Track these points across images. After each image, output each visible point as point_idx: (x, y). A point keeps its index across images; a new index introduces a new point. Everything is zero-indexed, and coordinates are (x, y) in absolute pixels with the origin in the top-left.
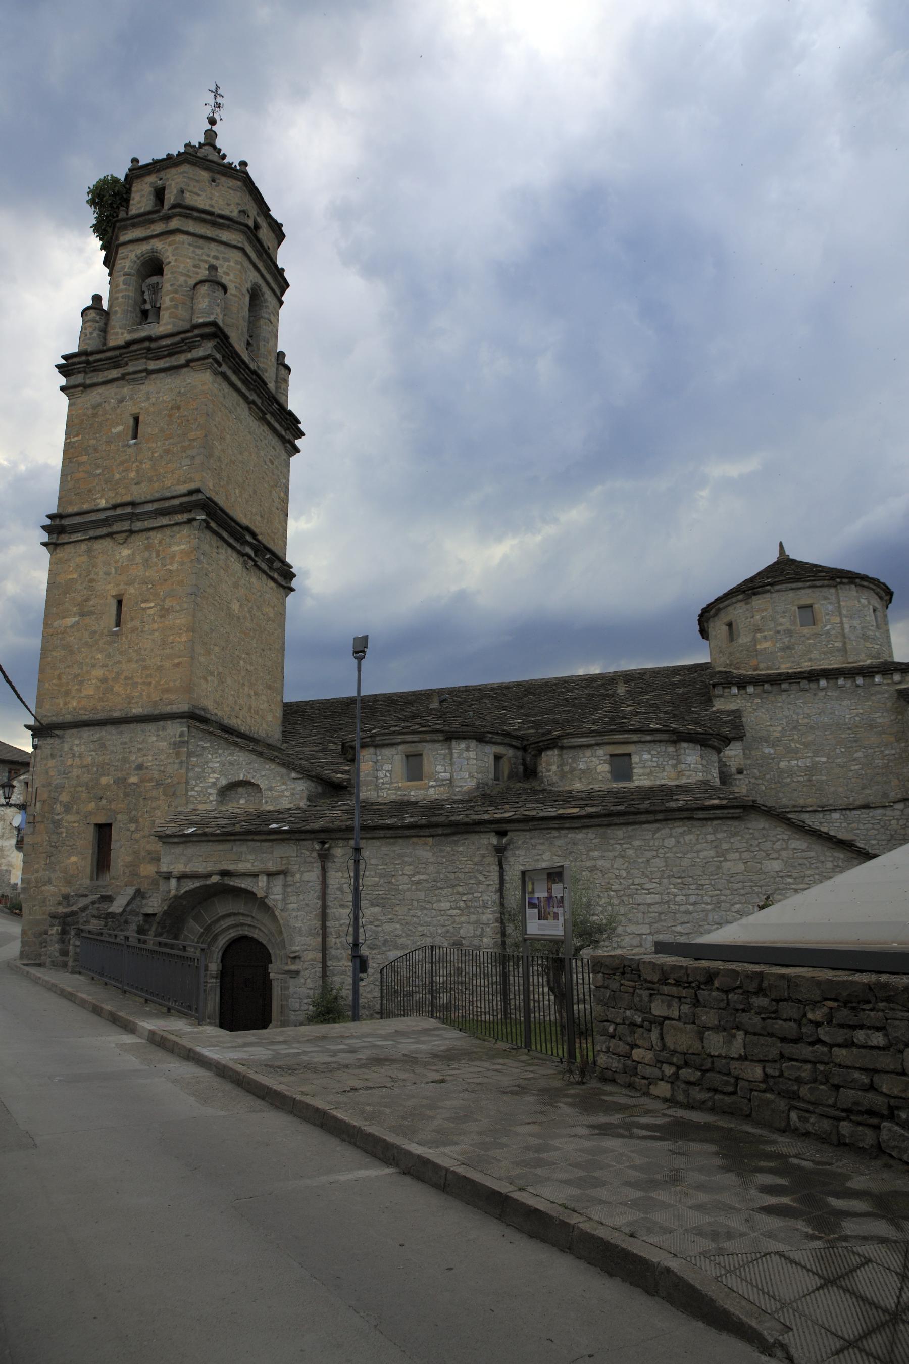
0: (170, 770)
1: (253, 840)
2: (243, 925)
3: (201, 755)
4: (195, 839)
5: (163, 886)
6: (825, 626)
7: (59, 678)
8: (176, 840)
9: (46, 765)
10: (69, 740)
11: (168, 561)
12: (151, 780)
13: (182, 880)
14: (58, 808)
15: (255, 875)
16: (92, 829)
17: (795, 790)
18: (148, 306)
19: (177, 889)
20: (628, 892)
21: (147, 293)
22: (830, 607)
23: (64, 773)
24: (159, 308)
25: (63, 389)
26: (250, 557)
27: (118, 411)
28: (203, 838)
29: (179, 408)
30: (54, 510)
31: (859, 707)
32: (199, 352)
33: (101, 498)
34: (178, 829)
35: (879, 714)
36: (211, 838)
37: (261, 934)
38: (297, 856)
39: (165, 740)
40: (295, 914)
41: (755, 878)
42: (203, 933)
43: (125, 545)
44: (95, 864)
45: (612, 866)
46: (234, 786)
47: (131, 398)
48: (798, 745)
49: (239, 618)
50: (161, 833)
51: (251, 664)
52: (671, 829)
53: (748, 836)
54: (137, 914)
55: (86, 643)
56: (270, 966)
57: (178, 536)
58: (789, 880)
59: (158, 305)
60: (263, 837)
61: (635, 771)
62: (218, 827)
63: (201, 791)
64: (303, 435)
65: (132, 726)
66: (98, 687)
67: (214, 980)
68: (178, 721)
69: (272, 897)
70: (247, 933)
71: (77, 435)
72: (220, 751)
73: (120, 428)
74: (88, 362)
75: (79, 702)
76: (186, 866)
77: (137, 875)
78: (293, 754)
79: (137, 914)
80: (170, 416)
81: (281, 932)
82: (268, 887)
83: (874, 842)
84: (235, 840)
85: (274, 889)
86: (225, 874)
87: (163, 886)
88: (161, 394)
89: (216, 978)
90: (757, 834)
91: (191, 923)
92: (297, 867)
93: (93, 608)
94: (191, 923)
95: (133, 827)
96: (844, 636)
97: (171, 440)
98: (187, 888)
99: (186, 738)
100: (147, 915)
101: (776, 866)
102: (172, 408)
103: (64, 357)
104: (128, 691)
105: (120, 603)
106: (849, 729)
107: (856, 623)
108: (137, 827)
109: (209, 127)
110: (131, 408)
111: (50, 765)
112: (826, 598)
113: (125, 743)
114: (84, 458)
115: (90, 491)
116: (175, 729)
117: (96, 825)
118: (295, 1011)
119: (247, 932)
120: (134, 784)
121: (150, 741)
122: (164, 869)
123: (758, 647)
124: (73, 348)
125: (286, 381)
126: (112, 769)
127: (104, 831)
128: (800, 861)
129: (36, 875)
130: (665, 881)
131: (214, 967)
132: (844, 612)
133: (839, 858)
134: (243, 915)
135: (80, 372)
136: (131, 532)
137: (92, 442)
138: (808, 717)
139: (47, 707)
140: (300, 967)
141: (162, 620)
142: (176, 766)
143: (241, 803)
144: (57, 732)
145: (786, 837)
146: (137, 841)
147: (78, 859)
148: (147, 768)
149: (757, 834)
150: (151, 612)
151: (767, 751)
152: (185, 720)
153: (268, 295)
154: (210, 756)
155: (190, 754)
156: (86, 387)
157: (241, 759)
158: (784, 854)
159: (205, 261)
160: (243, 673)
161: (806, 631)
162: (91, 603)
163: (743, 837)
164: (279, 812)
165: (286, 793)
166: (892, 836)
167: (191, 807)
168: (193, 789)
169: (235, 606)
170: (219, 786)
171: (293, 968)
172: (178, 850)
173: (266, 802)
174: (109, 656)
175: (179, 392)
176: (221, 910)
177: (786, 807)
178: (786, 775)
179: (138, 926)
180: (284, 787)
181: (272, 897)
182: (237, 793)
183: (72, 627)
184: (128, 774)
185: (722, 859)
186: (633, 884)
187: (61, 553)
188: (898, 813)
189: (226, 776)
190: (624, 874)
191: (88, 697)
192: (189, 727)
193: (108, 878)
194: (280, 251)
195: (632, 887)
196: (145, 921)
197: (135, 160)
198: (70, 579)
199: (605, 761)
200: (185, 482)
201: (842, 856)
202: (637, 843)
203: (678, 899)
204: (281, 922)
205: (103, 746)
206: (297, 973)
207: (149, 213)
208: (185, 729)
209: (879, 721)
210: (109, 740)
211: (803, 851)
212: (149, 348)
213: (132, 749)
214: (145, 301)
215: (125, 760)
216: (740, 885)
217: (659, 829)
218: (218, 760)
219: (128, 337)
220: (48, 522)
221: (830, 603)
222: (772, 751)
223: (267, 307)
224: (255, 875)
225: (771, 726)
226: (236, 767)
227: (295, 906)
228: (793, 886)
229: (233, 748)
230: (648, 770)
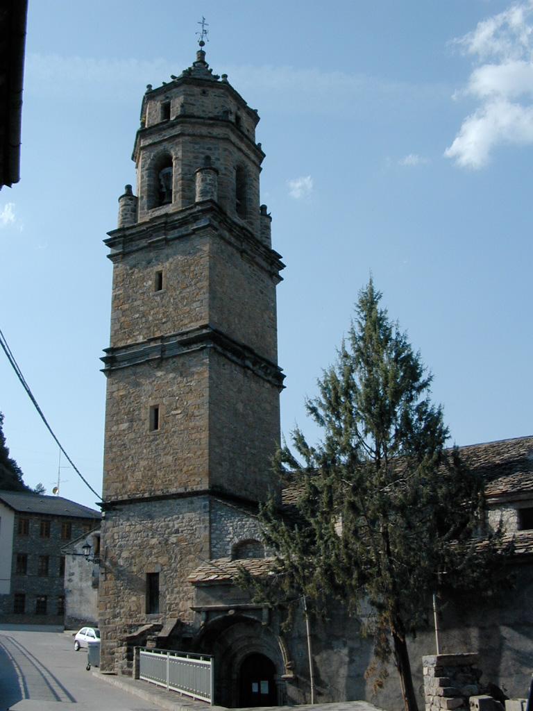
21: (162, 180)
25: (109, 256)
26: (249, 368)
30: (108, 346)
32: (202, 223)
33: (139, 334)
57: (195, 360)
64: (285, 266)
74: (124, 236)
78: (291, 515)
103: (109, 234)
109: (199, 48)
125: (268, 228)
135: (120, 243)
136: (167, 241)
144: (117, 507)
150: (179, 417)
153: (251, 167)
159: (202, 153)
160: (249, 456)
168: (215, 547)
169: (240, 407)
194: (257, 129)
197: (149, 86)
207: (161, 123)
212: (167, 224)
223: (250, 176)
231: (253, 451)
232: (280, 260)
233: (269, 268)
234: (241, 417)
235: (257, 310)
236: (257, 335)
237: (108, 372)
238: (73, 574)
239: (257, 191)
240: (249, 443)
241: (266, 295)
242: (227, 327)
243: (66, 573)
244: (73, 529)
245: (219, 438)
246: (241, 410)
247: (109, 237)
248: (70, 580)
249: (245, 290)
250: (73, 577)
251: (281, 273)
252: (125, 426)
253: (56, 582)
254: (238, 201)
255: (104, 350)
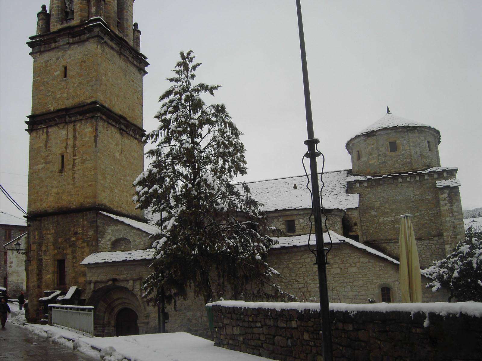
1: (126, 265)
2: (125, 303)
6: (402, 151)
7: (37, 193)
11: (84, 136)
17: (387, 232)
18: (68, 10)
20: (290, 283)
22: (405, 142)
24: (73, 11)
25: (30, 54)
27: (57, 64)
29: (85, 62)
31: (418, 191)
33: (51, 107)
35: (427, 194)
38: (146, 271)
41: (345, 275)
43: (64, 129)
45: (283, 271)
47: (63, 58)
48: (388, 211)
49: (119, 160)
51: (127, 181)
52: (308, 254)
53: (342, 257)
55: (49, 177)
58: (360, 276)
59: (73, 9)
61: (296, 228)
63: (104, 243)
66: (55, 197)
67: (113, 328)
71: (38, 77)
73: (58, 73)
76: (98, 277)
80: (81, 66)
82: (134, 286)
83: (424, 256)
86: (114, 280)
88: (76, 55)
90: (346, 256)
93: (51, 160)
96: (411, 156)
97: (82, 78)
101: (354, 270)
102: (82, 62)
103: (30, 38)
104: (69, 198)
105: (63, 157)
106: (413, 202)
107: (417, 149)
108: (76, 261)
110: (62, 62)
112: (403, 137)
114: (42, 88)
115: (46, 103)
119: (126, 306)
122: (88, 279)
123: (370, 162)
124: (34, 32)
128: (365, 268)
129: (32, 284)
130: (306, 278)
132: (411, 144)
133: (382, 266)
134: (125, 298)
137: (45, 80)
138: (393, 196)
139: (33, 207)
141: (82, 164)
145: (359, 257)
149: (346, 256)
151: (373, 213)
156: (41, 52)
157: (121, 228)
158: (358, 265)
160: (123, 186)
161: (393, 154)
162: (50, 157)
163: (340, 257)
166: (432, 253)
169: (117, 155)
170: (111, 241)
174: (59, 182)
175: (85, 54)
177: (381, 240)
178: (382, 225)
182: (120, 243)
183: (42, 169)
185: (331, 267)
186: (292, 279)
187: (34, 134)
188: (436, 242)
190: (288, 275)
191: (51, 202)
195: (291, 281)
198: (39, 146)
199: (283, 223)
200: (89, 98)
201: (383, 265)
202: (293, 261)
203: (311, 285)
208: (95, 215)
209: (427, 197)
211: (366, 263)
214: (66, 8)
216: (338, 279)
217: (303, 255)
218: (111, 229)
219: (59, 27)
220: (28, 119)
221: (405, 140)
222: (376, 214)
225: (375, 201)
226: (119, 232)
228: (362, 279)
230: (302, 227)
231: (126, 183)
232: (146, 60)
233: (138, 65)
234: (118, 161)
235: (130, 93)
236: (129, 109)
237: (30, 131)
238: (12, 263)
239: (131, 14)
240: (123, 178)
241: (136, 83)
242: (109, 103)
243: (8, 262)
244: (12, 233)
245: (103, 174)
246: (118, 157)
247: (30, 41)
248: (10, 267)
249: (121, 79)
250: (12, 265)
251: (146, 69)
252: (41, 166)
253: (2, 268)
254: (118, 20)
255: (27, 117)
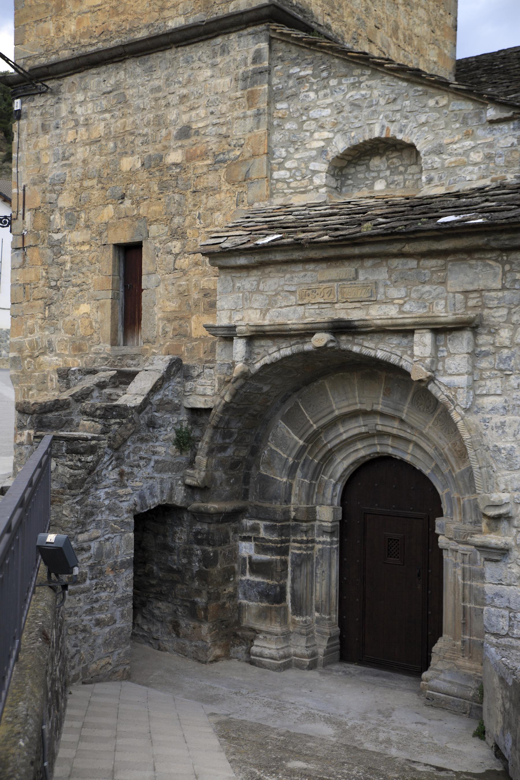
0: (238, 131)
2: (381, 434)
3: (295, 95)
4: (279, 257)
5: (221, 356)
8: (242, 261)
9: (36, 145)
10: (67, 95)
12: (204, 155)
13: (257, 343)
14: (58, 219)
15: (406, 332)
16: (110, 253)
19: (247, 361)
23: (64, 158)
28: (296, 255)
34: (245, 239)
36: (312, 254)
37: (419, 454)
38: (504, 288)
39: (228, 74)
40: (497, 419)
42: (303, 449)
44: (119, 316)
46: (362, 153)
50: (216, 248)
54: (176, 409)
56: (438, 521)
60: (424, 246)
62: (326, 229)
63: (297, 169)
65: (169, 54)
68: (250, 30)
69: (445, 380)
70: (390, 451)
72: (333, 82)
75: (79, 23)
76: (264, 313)
77: (186, 335)
79: (176, 409)
81: (462, 454)
82: (436, 359)
84: (362, 257)
85: (449, 362)
86: (340, 328)
87: (221, 356)
89: (331, 534)
91: (282, 428)
92: (504, 312)
94: (282, 428)
95: (176, 246)
98: (267, 360)
99: (266, 64)
100: (194, 411)
108: (184, 246)
111: (41, 145)
113: (158, 89)
116: (245, 48)
117: (118, 247)
118: (497, 635)
119: (389, 448)
120: (176, 165)
121: (201, 79)
122: (224, 321)
126: (139, 141)
127: (129, 255)
129: (30, 337)
131: (327, 514)
134: (382, 415)
140: (509, 540)
142: (249, 123)
143: (379, 185)
146: (185, 272)
147: (92, 310)
148: (197, 133)
152: (262, 27)
154: (312, 95)
155: (274, 97)
157: (376, 93)
164: (458, 195)
165: (475, 157)
167: (278, 201)
168: (281, 166)
170: (331, 155)
171: (494, 539)
172: (248, 282)
173: (430, 180)
176: (339, 404)
179: (178, 432)
180: (468, 143)
181: (445, 380)
184: (165, 148)
189: (345, 133)
192: (271, 40)
193: (141, 342)
196: (193, 422)
204: (466, 436)
205: (123, 100)
206: (503, 552)
208: (264, 45)
210: (132, 86)
213: (171, 98)
215: (159, 122)
218: (329, 100)
224: (406, 332)
226: (366, 112)
227: (499, 401)
229: (357, 72)
